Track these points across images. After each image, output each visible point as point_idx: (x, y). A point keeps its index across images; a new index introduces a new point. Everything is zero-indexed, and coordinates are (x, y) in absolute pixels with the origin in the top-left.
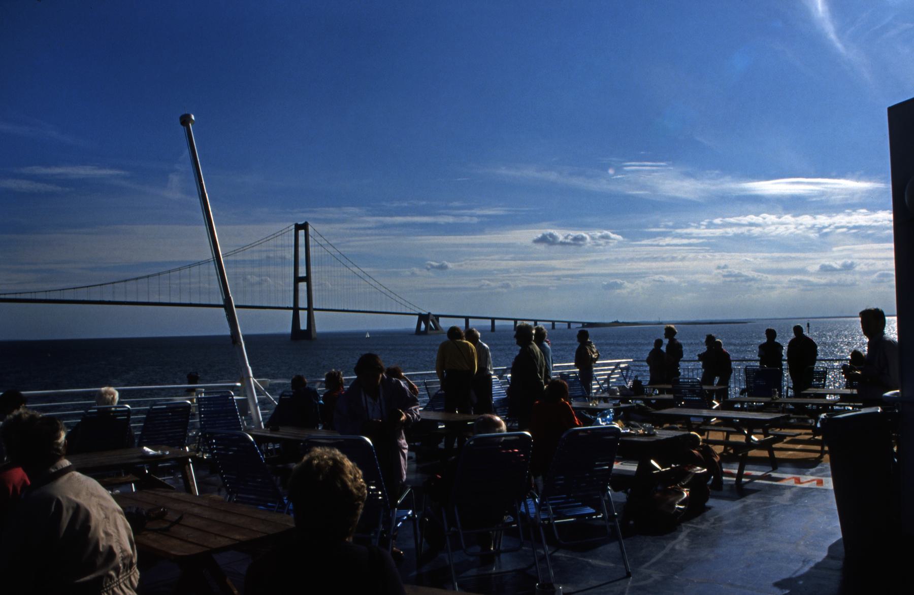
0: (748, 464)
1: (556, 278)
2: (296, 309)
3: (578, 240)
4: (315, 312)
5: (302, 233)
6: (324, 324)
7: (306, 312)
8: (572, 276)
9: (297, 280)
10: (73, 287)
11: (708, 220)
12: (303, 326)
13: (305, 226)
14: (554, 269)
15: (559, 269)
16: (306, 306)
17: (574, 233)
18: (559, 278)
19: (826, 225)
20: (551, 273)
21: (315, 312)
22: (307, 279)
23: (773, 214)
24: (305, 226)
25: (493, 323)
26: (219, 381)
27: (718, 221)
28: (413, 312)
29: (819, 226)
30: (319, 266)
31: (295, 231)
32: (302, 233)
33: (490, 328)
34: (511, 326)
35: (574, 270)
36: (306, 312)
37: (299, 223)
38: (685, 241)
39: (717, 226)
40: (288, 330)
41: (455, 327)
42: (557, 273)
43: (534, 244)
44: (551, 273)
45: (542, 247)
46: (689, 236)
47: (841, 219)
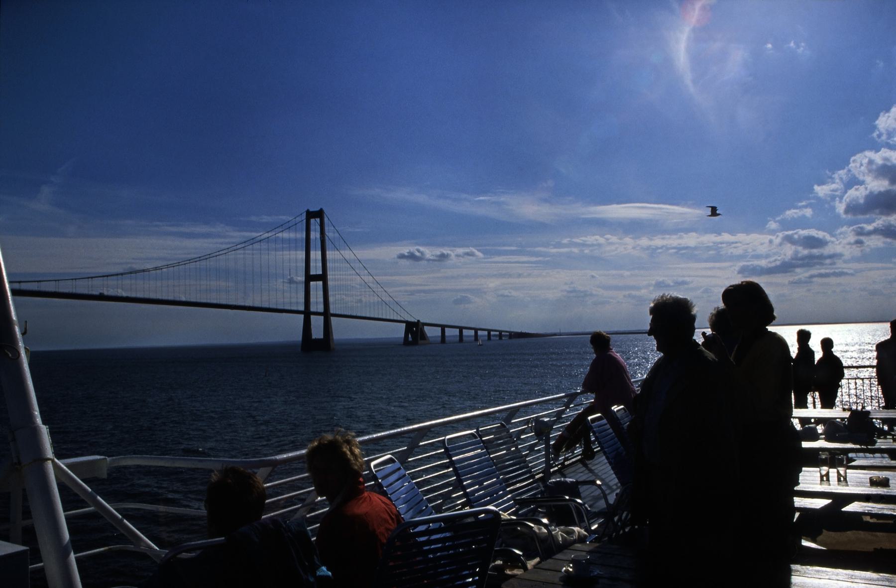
0: (794, 505)
1: (409, 293)
2: (307, 313)
3: (443, 257)
4: (332, 318)
5: (315, 223)
6: (342, 331)
7: (322, 317)
8: (424, 291)
9: (309, 278)
10: (87, 277)
11: (569, 239)
12: (317, 332)
13: (320, 214)
14: (406, 285)
15: (411, 285)
16: (321, 309)
17: (438, 251)
18: (412, 293)
19: (659, 246)
20: (402, 288)
21: (332, 318)
22: (323, 277)
23: (615, 236)
24: (320, 214)
25: (443, 332)
26: (528, 447)
27: (565, 241)
28: (399, 318)
29: (654, 247)
30: (216, 280)
31: (306, 221)
32: (315, 223)
33: (440, 339)
34: (454, 336)
35: (425, 285)
36: (322, 317)
37: (311, 210)
38: (534, 259)
39: (565, 246)
40: (298, 337)
41: (799, 330)
42: (408, 288)
43: (399, 260)
44: (402, 288)
45: (404, 262)
46: (544, 255)
47: (673, 241)
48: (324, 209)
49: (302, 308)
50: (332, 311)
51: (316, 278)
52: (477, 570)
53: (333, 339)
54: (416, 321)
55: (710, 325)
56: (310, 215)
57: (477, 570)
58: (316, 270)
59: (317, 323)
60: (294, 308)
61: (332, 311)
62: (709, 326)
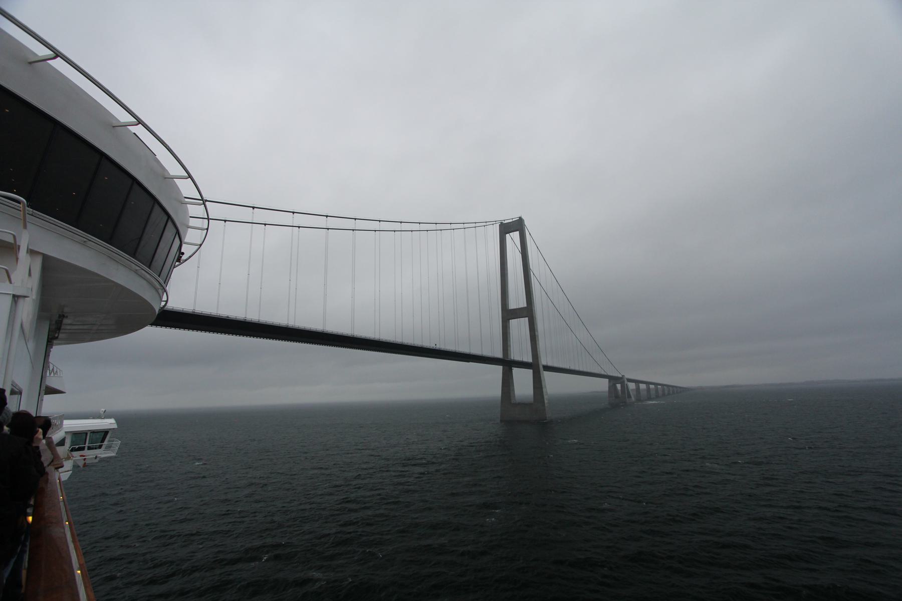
5: (513, 239)
9: (508, 314)
13: (518, 225)
22: (528, 312)
24: (518, 225)
48: (523, 218)
49: (210, 220)
50: (210, 218)
51: (517, 314)
52: (7, 110)
53: (514, 394)
54: (621, 376)
55: (22, 411)
56: (505, 229)
57: (7, 110)
58: (517, 300)
59: (523, 382)
60: (487, 353)
61: (210, 218)
62: (21, 409)
